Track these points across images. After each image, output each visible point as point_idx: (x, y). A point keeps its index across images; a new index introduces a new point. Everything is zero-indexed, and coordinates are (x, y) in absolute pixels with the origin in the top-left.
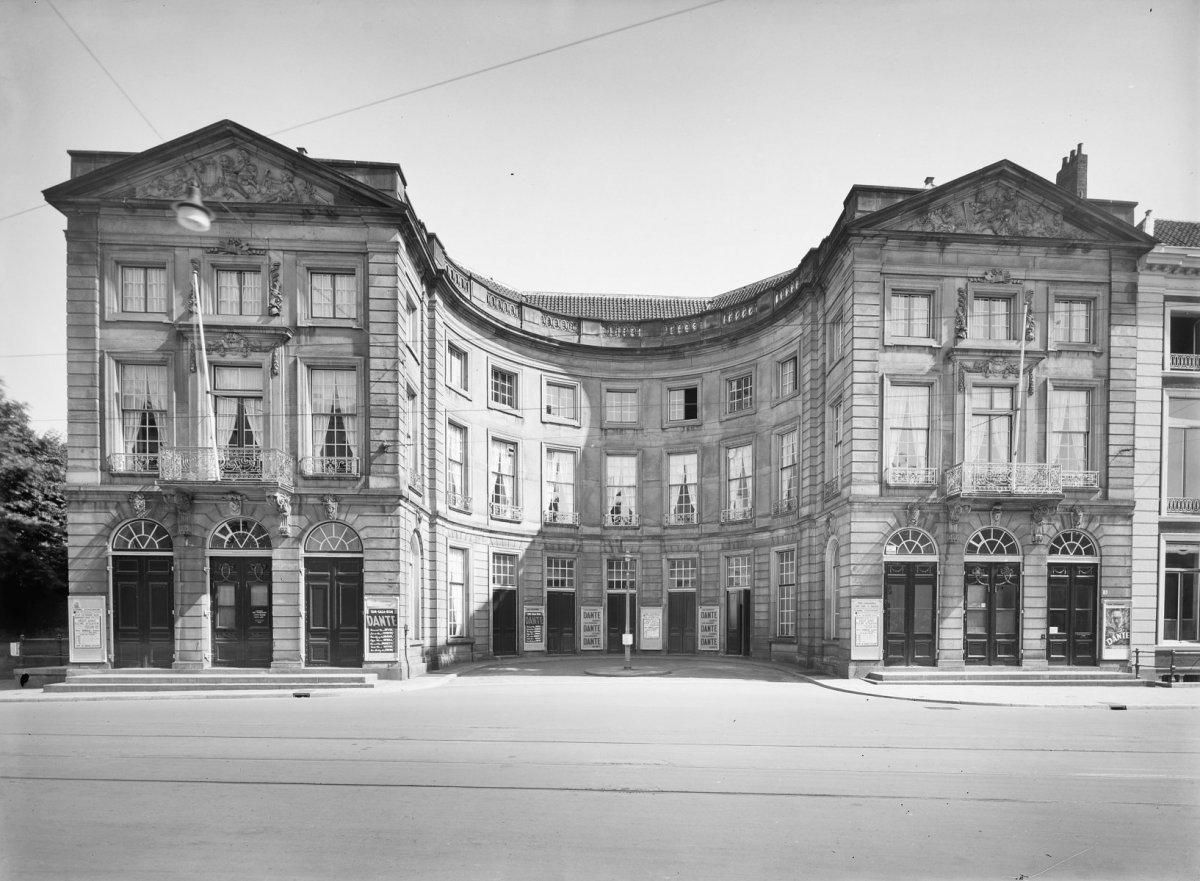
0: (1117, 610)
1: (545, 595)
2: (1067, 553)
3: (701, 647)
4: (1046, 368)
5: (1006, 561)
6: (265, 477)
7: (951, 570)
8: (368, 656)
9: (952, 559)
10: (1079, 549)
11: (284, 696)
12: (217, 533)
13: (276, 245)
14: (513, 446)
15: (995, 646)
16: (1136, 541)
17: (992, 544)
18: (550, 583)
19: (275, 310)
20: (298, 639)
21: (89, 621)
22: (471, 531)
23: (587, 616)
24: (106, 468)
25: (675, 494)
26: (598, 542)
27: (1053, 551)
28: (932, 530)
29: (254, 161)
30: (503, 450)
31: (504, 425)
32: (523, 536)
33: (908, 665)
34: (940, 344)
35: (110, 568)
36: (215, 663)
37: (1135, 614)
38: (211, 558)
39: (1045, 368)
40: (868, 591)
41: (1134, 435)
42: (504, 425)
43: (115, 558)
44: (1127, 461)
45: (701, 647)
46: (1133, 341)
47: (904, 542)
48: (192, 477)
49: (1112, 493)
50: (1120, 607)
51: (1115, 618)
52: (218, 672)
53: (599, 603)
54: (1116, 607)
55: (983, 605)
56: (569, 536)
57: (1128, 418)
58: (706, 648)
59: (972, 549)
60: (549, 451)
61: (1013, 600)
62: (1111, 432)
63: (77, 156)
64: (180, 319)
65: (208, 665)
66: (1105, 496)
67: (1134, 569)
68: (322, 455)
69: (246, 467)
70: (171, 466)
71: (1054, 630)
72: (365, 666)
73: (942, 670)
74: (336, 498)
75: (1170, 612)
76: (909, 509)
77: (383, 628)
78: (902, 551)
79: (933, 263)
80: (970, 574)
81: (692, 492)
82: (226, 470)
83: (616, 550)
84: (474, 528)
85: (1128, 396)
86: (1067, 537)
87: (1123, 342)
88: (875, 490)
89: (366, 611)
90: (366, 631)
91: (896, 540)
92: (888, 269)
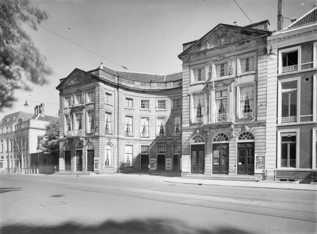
0: (260, 157)
1: (157, 155)
2: (245, 139)
3: (167, 169)
4: (237, 82)
5: (224, 143)
6: (228, 121)
7: (208, 146)
8: (95, 169)
9: (208, 143)
10: (200, 140)
11: (75, 176)
12: (215, 137)
13: (83, 89)
14: (148, 119)
15: (222, 168)
16: (267, 134)
17: (220, 138)
18: (158, 153)
19: (231, 73)
20: (86, 166)
21: (186, 163)
22: (134, 141)
23: (168, 161)
24: (190, 122)
25: (175, 127)
26: (171, 141)
27: (240, 139)
28: (203, 135)
29: (81, 74)
30: (146, 120)
31: (145, 114)
32: (150, 141)
33: (197, 174)
34: (205, 82)
35: (64, 153)
36: (77, 170)
37: (266, 158)
38: (76, 150)
39: (237, 82)
40: (186, 153)
41: (266, 98)
42: (145, 114)
43: (65, 151)
44: (264, 107)
45: (167, 169)
46: (265, 67)
47: (196, 139)
48: (210, 123)
49: (258, 119)
50: (261, 156)
51: (259, 160)
52: (192, 175)
53: (170, 157)
54: (259, 156)
55: (218, 156)
56: (163, 140)
57: (265, 93)
58: (168, 169)
59: (215, 140)
60: (158, 118)
61: (226, 155)
62: (258, 98)
63: (61, 80)
64: (207, 81)
65: (86, 171)
66: (256, 120)
67: (267, 143)
68: (243, 112)
69: (224, 118)
70: (205, 121)
71: (240, 164)
72: (94, 171)
73: (205, 175)
74: (91, 138)
75: (284, 155)
76: (195, 130)
77: (153, 163)
78: (196, 142)
79: (204, 59)
80: (215, 147)
81: (164, 128)
82: (219, 120)
83: (175, 143)
84: (134, 140)
85: (265, 86)
86: (244, 134)
87: (262, 68)
88: (188, 125)
89: (94, 160)
90: (94, 164)
91: (194, 139)
92: (191, 64)
